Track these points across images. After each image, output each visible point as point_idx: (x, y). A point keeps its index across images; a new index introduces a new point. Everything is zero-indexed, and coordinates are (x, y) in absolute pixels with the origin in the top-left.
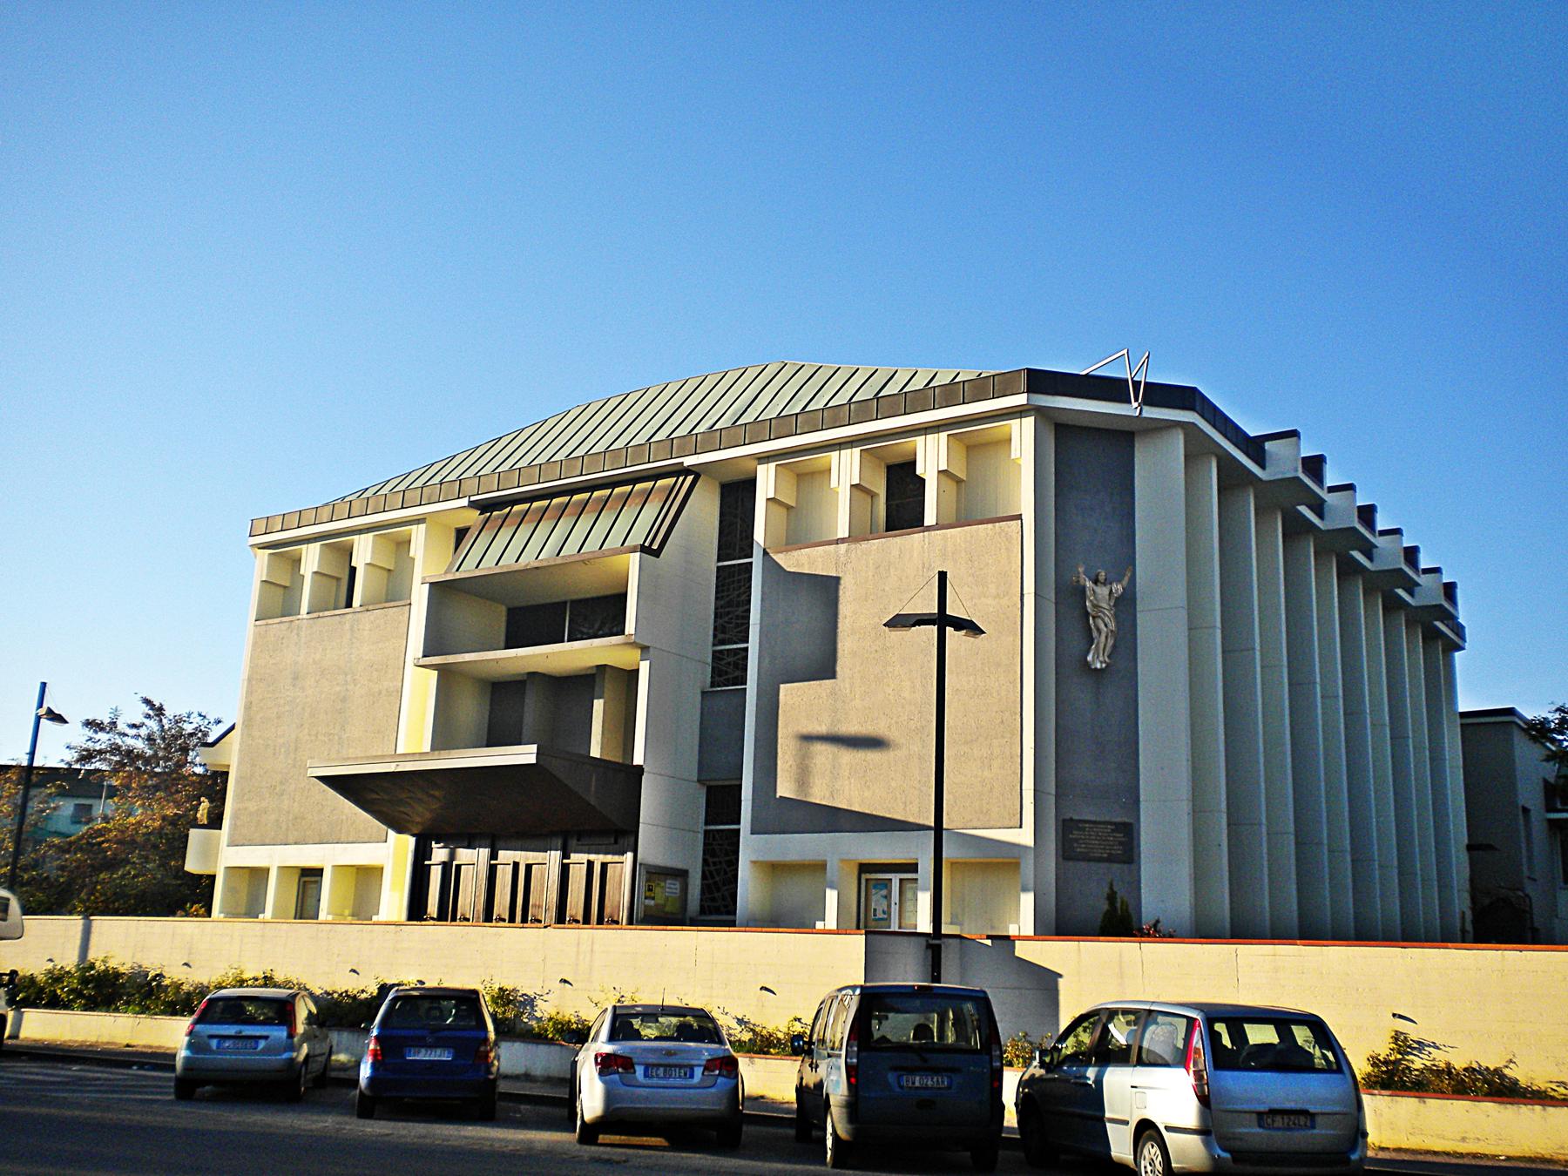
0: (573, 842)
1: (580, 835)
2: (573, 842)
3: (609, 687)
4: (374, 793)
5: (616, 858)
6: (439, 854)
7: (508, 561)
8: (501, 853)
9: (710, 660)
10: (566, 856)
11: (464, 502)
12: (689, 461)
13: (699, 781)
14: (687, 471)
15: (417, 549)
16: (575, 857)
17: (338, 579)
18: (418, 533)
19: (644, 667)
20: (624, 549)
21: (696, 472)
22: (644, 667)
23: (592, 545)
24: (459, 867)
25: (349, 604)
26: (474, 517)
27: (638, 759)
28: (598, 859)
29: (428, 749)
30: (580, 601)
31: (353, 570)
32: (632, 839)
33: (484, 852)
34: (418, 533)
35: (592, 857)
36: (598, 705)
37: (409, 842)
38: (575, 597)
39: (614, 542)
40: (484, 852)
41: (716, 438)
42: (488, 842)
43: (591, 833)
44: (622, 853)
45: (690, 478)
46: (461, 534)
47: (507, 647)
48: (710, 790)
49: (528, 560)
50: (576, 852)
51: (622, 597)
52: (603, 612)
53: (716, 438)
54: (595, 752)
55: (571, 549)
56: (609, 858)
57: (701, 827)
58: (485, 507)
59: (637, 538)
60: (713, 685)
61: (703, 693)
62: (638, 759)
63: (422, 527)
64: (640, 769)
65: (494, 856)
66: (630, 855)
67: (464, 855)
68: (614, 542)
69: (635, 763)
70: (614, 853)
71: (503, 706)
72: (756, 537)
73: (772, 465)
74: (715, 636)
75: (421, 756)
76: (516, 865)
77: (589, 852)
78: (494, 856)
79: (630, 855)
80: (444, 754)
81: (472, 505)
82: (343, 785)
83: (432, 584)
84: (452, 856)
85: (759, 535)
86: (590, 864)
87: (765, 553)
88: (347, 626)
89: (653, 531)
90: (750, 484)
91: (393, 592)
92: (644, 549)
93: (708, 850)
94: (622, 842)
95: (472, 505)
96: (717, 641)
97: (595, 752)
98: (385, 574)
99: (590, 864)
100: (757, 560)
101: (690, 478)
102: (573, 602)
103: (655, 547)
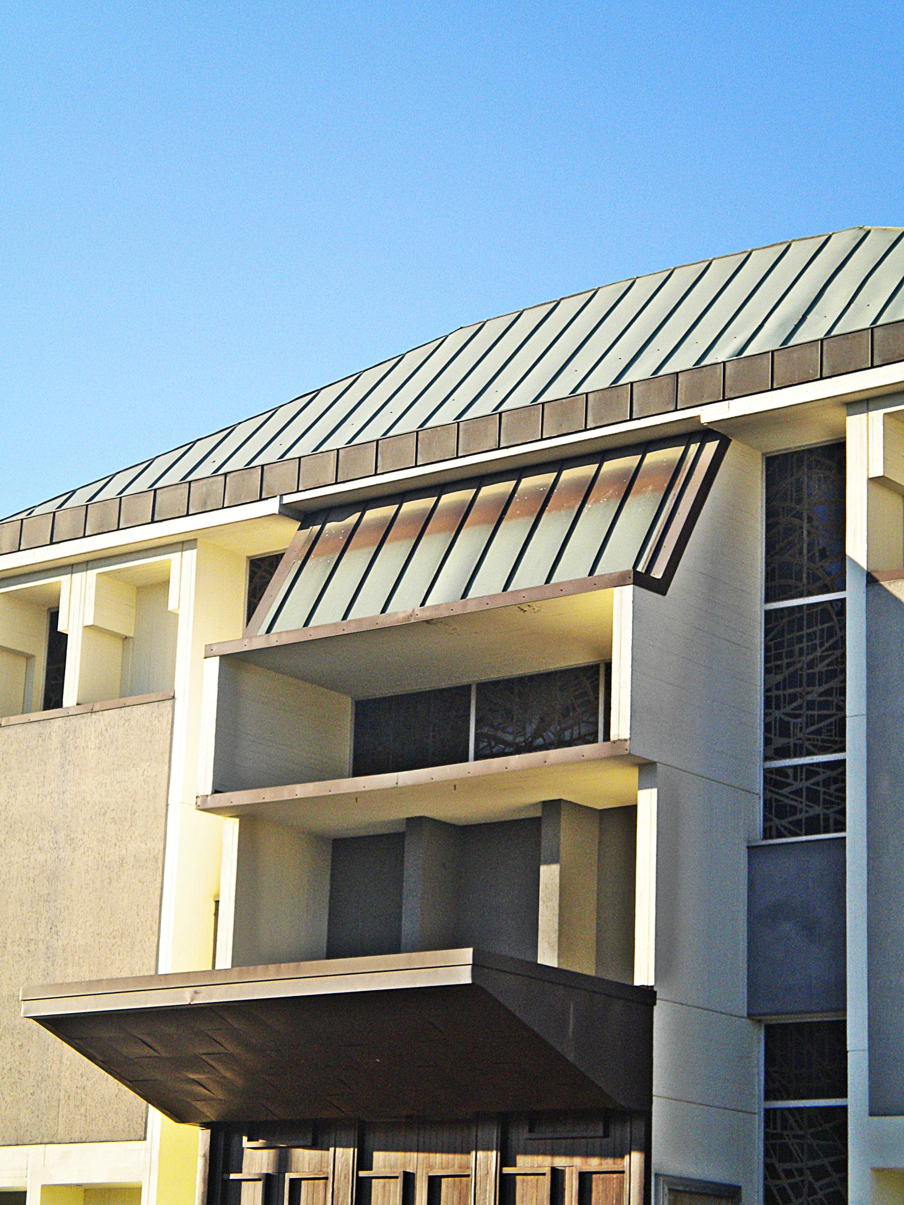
0: (520, 1135)
1: (534, 1120)
2: (520, 1135)
3: (568, 835)
4: (142, 1048)
5: (609, 1164)
6: (257, 1159)
7: (367, 609)
8: (379, 1157)
9: (759, 786)
10: (506, 1159)
11: (272, 506)
12: (710, 414)
13: (750, 1015)
14: (705, 433)
15: (182, 597)
16: (524, 1163)
17: (29, 658)
18: (182, 568)
19: (647, 804)
20: (594, 579)
21: (720, 434)
22: (647, 804)
23: (531, 575)
24: (295, 1184)
25: (53, 698)
26: (288, 536)
27: (644, 973)
28: (573, 1166)
29: (229, 966)
30: (496, 683)
31: (57, 644)
32: (639, 1126)
33: (346, 1155)
34: (182, 568)
35: (560, 1162)
36: (549, 875)
37: (197, 1139)
38: (484, 678)
39: (574, 566)
40: (346, 1155)
41: (775, 369)
42: (353, 1135)
43: (555, 1117)
44: (620, 1153)
45: (711, 447)
46: (262, 570)
47: (356, 773)
48: (770, 1031)
49: (405, 605)
50: (525, 1153)
51: (598, 673)
52: (566, 700)
53: (775, 369)
54: (547, 956)
55: (489, 583)
56: (594, 1164)
57: (759, 1104)
58: (307, 515)
59: (621, 556)
60: (767, 834)
61: (752, 850)
62: (644, 973)
63: (190, 555)
64: (648, 995)
65: (364, 1162)
66: (636, 1158)
67: (305, 1160)
68: (574, 566)
69: (637, 982)
70: (603, 1155)
71: (358, 883)
72: (849, 551)
73: (877, 416)
74: (767, 741)
75: (212, 976)
76: (409, 1180)
77: (553, 1153)
78: (364, 1162)
79: (636, 1158)
80: (260, 971)
81: (288, 511)
82: (57, 1025)
83: (222, 657)
84: (283, 1163)
85: (857, 547)
86: (557, 1176)
87: (871, 580)
88: (54, 742)
89: (649, 546)
90: (835, 452)
91: (139, 680)
92: (642, 580)
93: (776, 1148)
94: (620, 1133)
95: (288, 511)
96: (773, 751)
97: (547, 956)
98: (119, 644)
99: (557, 1176)
100: (854, 595)
101: (711, 447)
102: (481, 686)
103: (658, 573)
